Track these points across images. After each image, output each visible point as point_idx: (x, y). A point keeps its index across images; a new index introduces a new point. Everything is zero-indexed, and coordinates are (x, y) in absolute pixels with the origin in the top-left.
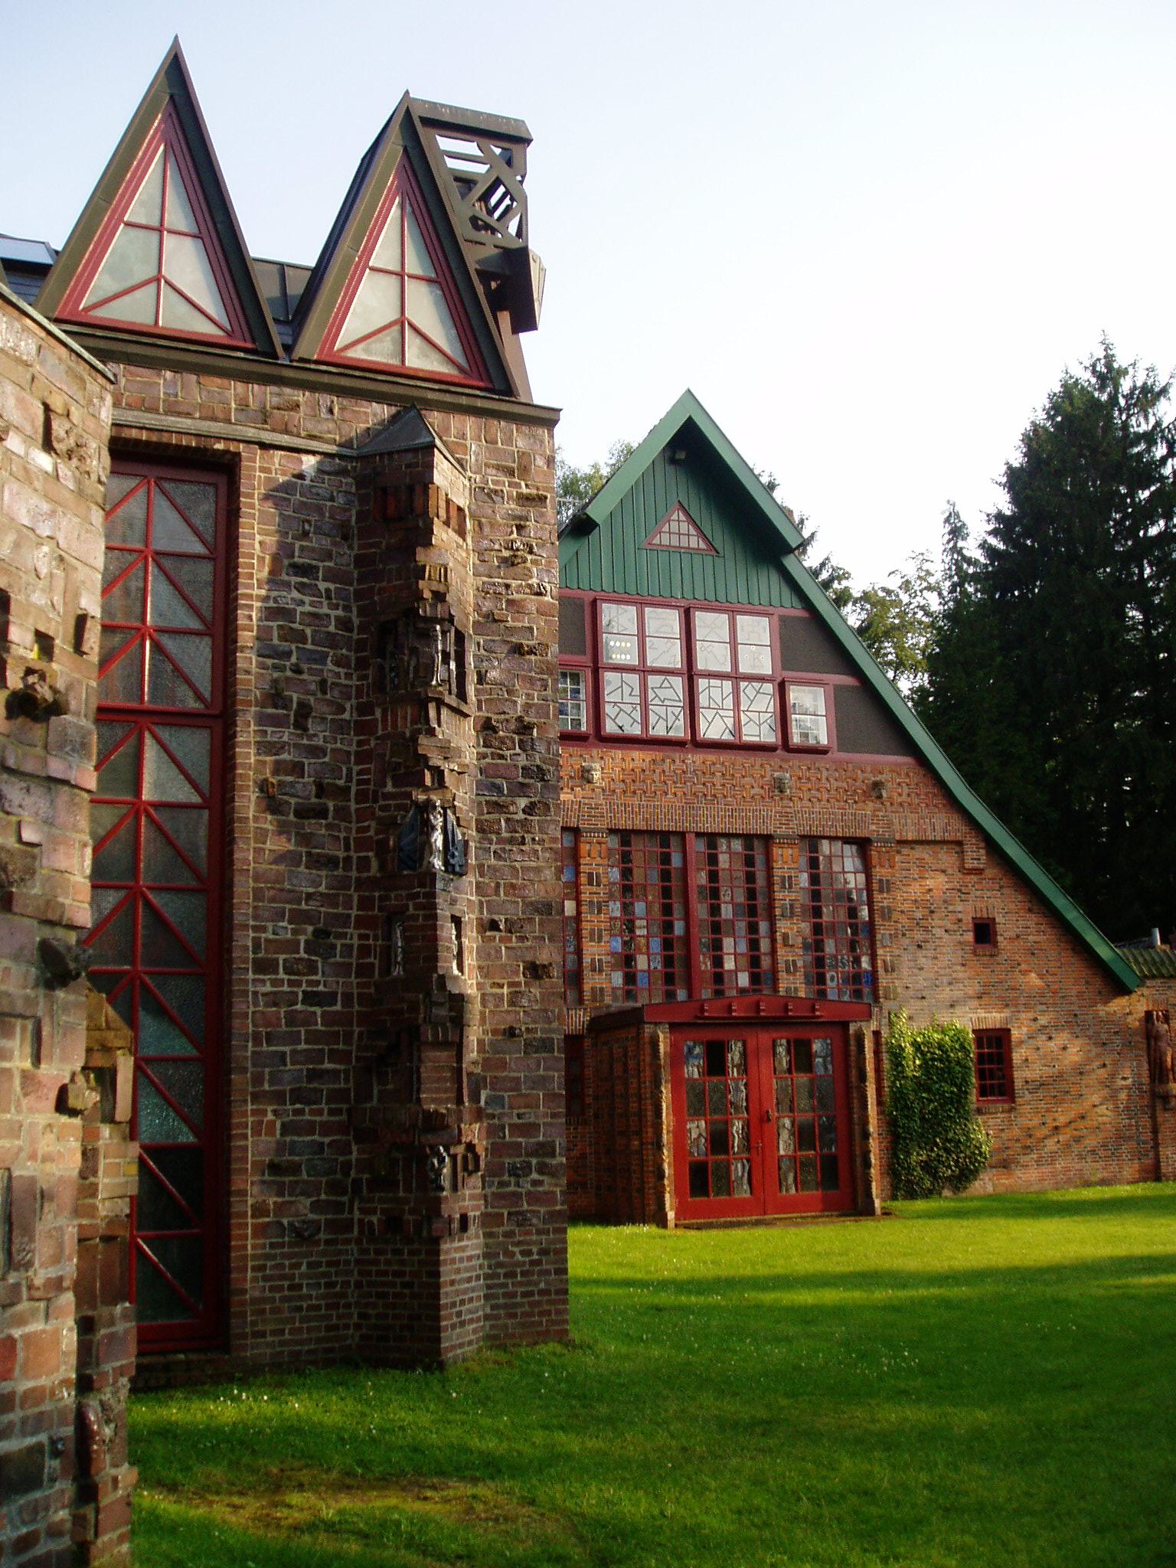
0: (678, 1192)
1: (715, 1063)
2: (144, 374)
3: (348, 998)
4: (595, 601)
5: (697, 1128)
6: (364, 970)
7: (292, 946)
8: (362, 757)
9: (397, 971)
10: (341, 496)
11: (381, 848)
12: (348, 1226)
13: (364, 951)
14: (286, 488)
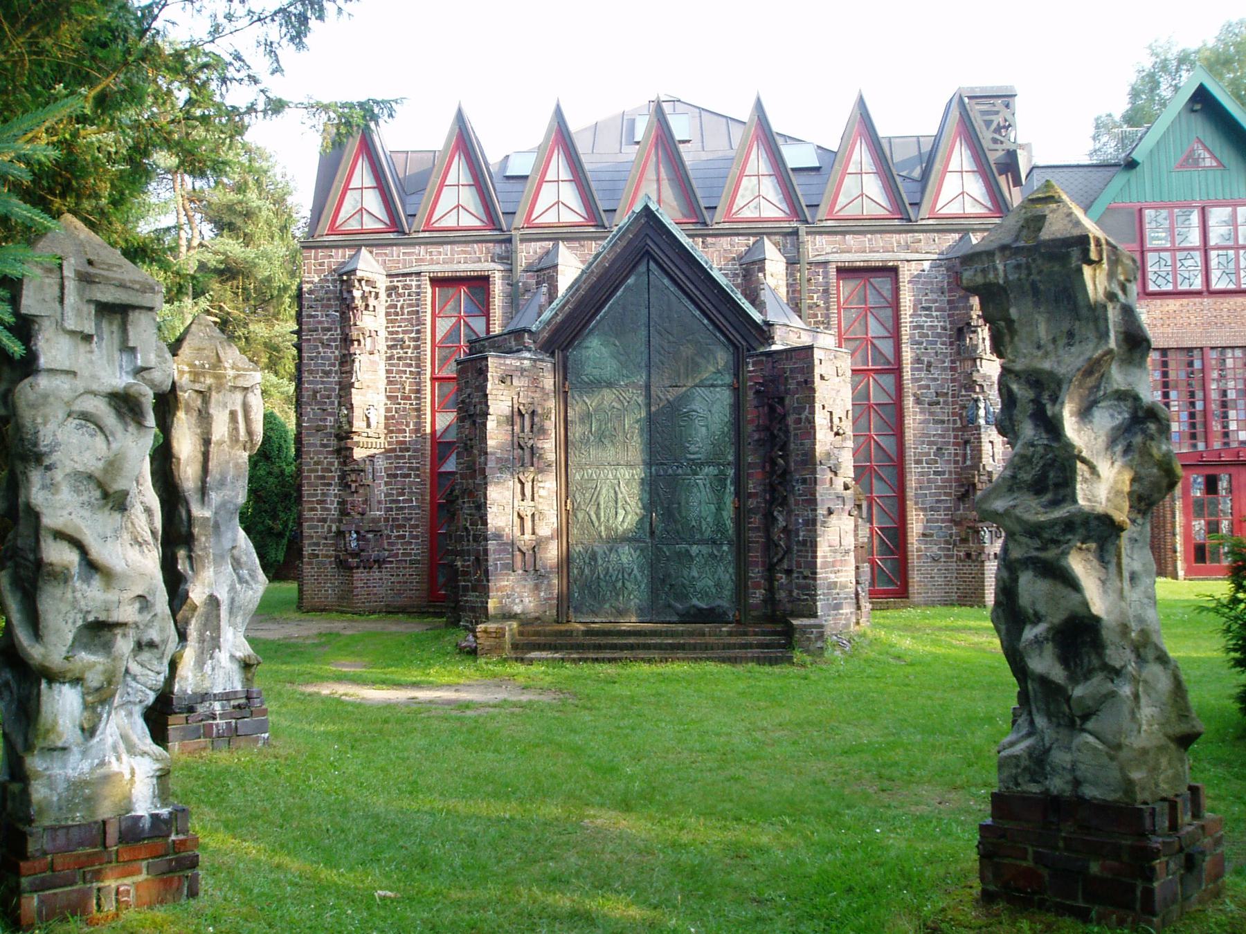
0: (1186, 560)
1: (1211, 485)
2: (861, 238)
3: (950, 472)
4: (1140, 210)
5: (1199, 525)
6: (956, 462)
7: (928, 454)
8: (953, 380)
9: (968, 463)
10: (941, 277)
11: (961, 416)
12: (952, 556)
13: (956, 455)
14: (918, 276)
